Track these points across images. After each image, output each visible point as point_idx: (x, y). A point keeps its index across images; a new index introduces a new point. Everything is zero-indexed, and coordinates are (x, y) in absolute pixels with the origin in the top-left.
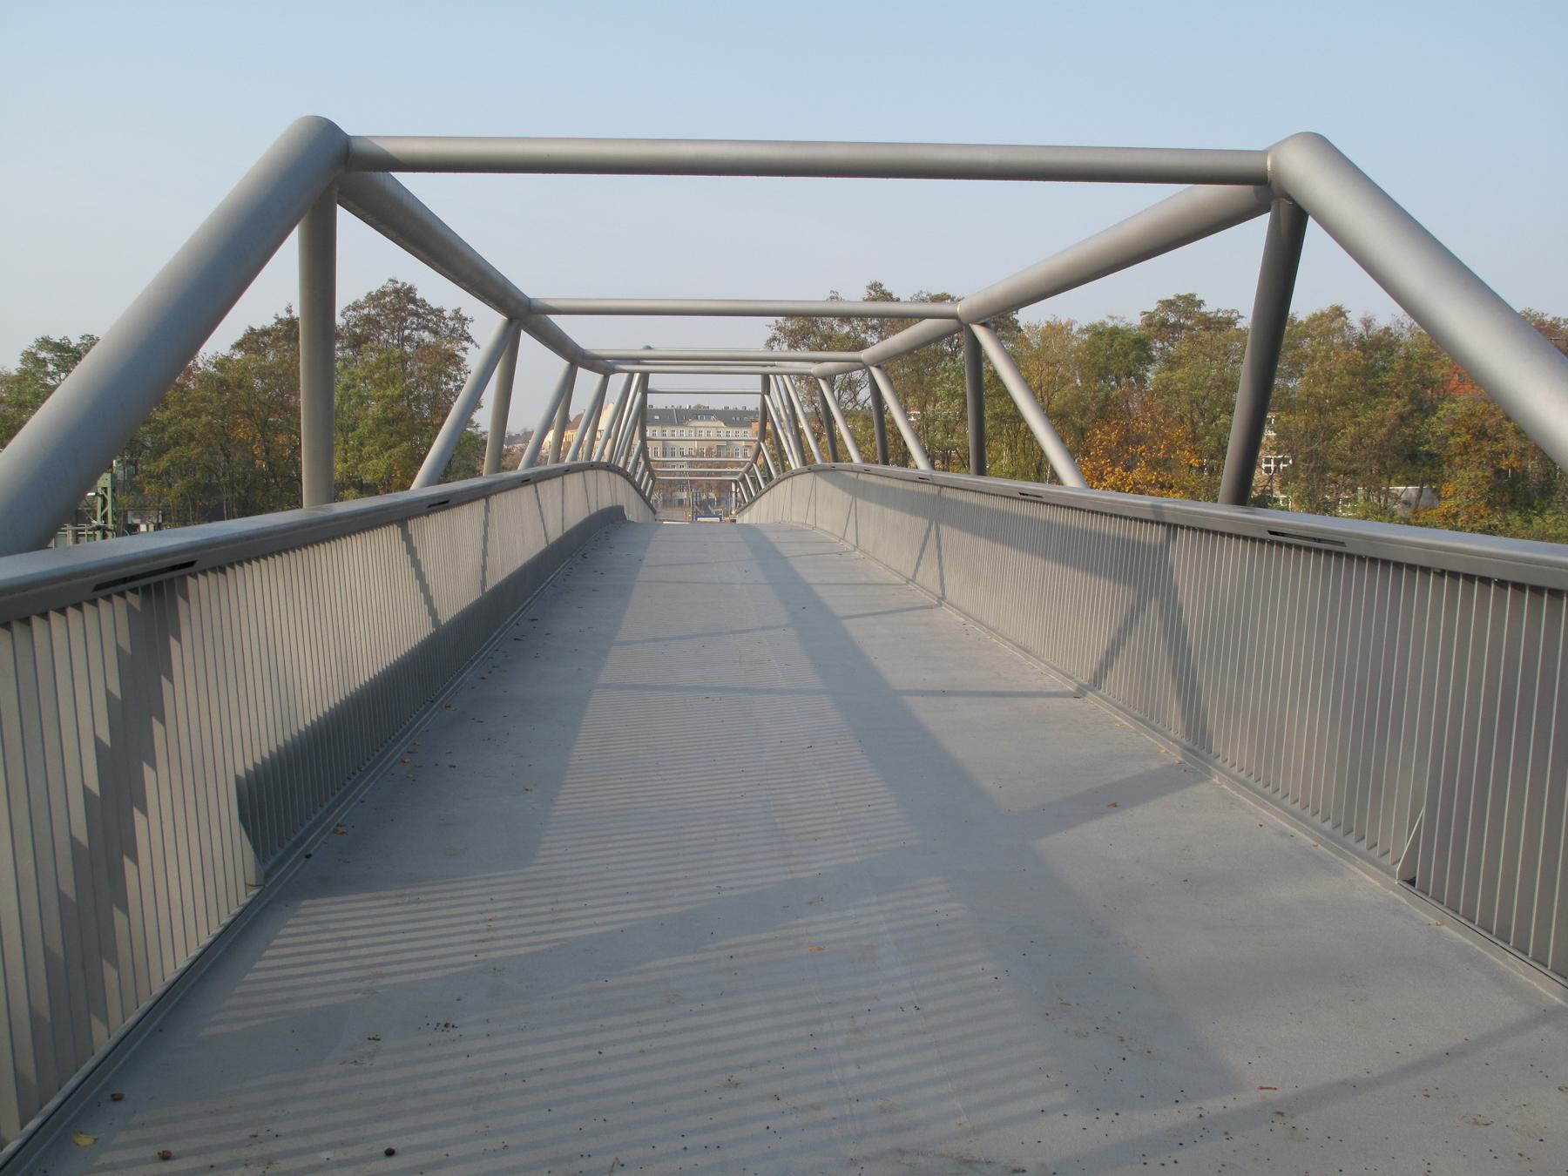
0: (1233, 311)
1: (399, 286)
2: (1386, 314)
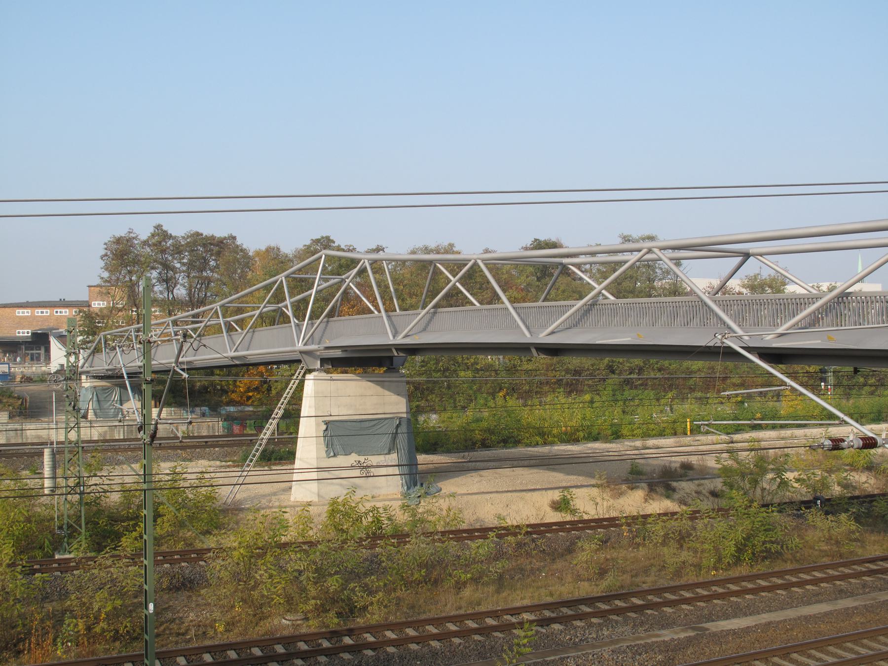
0: (351, 246)
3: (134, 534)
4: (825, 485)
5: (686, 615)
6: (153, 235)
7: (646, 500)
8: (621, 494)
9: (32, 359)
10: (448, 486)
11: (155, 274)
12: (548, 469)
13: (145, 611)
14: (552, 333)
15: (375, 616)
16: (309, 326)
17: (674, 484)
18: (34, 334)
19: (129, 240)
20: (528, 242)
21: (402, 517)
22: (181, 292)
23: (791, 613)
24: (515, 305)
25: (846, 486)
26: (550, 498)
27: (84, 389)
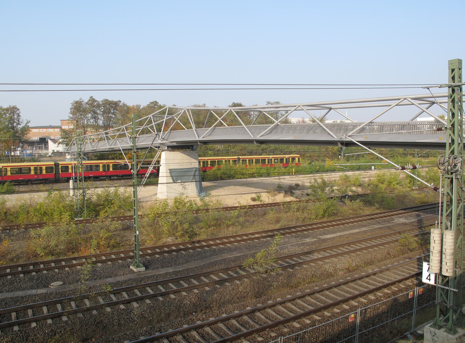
3: (104, 211)
4: (346, 191)
5: (312, 234)
6: (89, 100)
7: (284, 197)
8: (275, 195)
9: (39, 148)
10: (214, 193)
11: (90, 115)
12: (248, 186)
13: (135, 234)
14: (262, 136)
15: (203, 237)
16: (163, 134)
17: (294, 191)
18: (40, 138)
19: (81, 102)
20: (231, 104)
21: (199, 203)
22: (101, 123)
23: (347, 233)
24: (248, 126)
25: (352, 191)
26: (251, 197)
27: (67, 159)
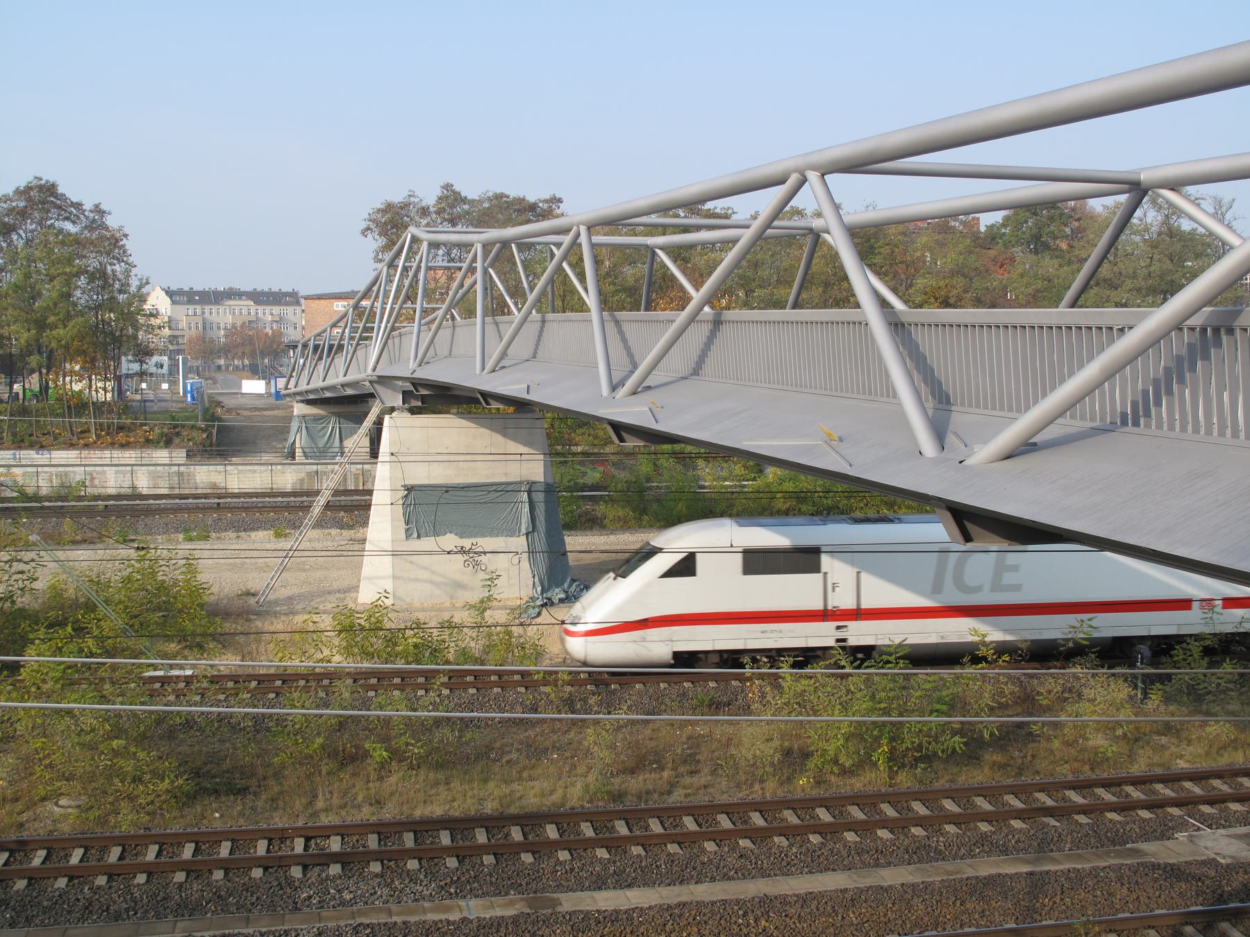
0: (729, 208)
1: (43, 182)
2: (684, 555)
